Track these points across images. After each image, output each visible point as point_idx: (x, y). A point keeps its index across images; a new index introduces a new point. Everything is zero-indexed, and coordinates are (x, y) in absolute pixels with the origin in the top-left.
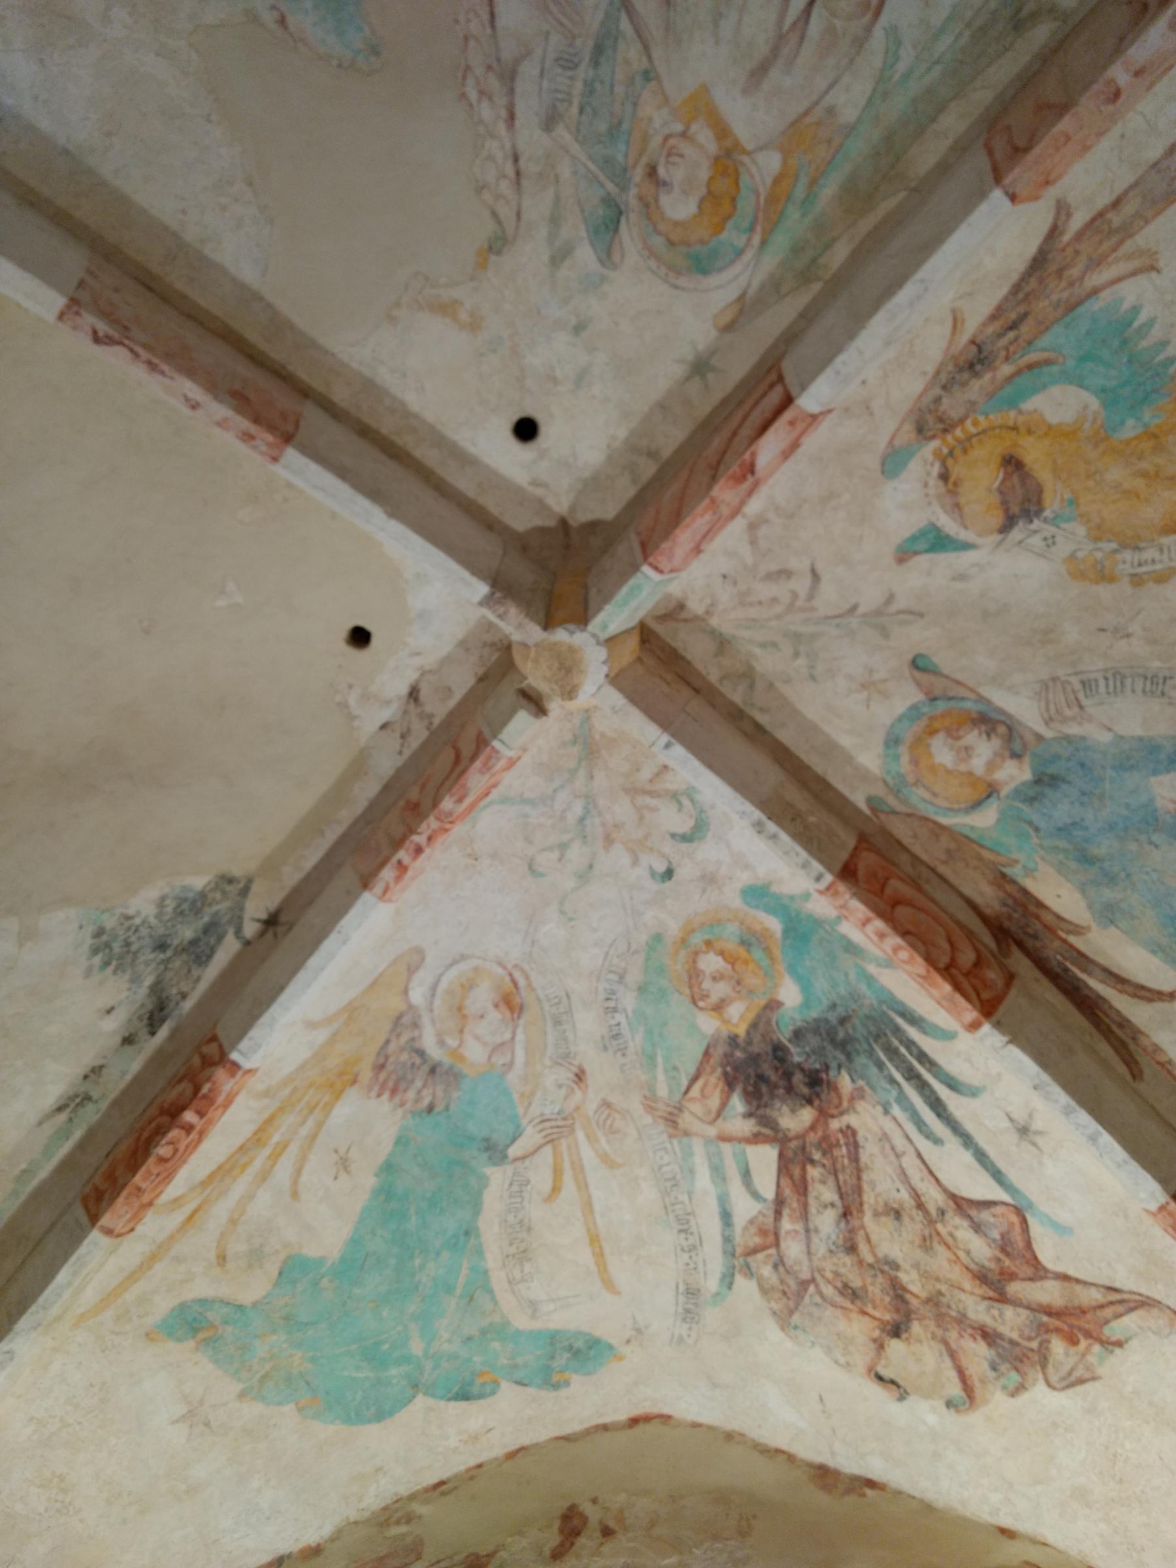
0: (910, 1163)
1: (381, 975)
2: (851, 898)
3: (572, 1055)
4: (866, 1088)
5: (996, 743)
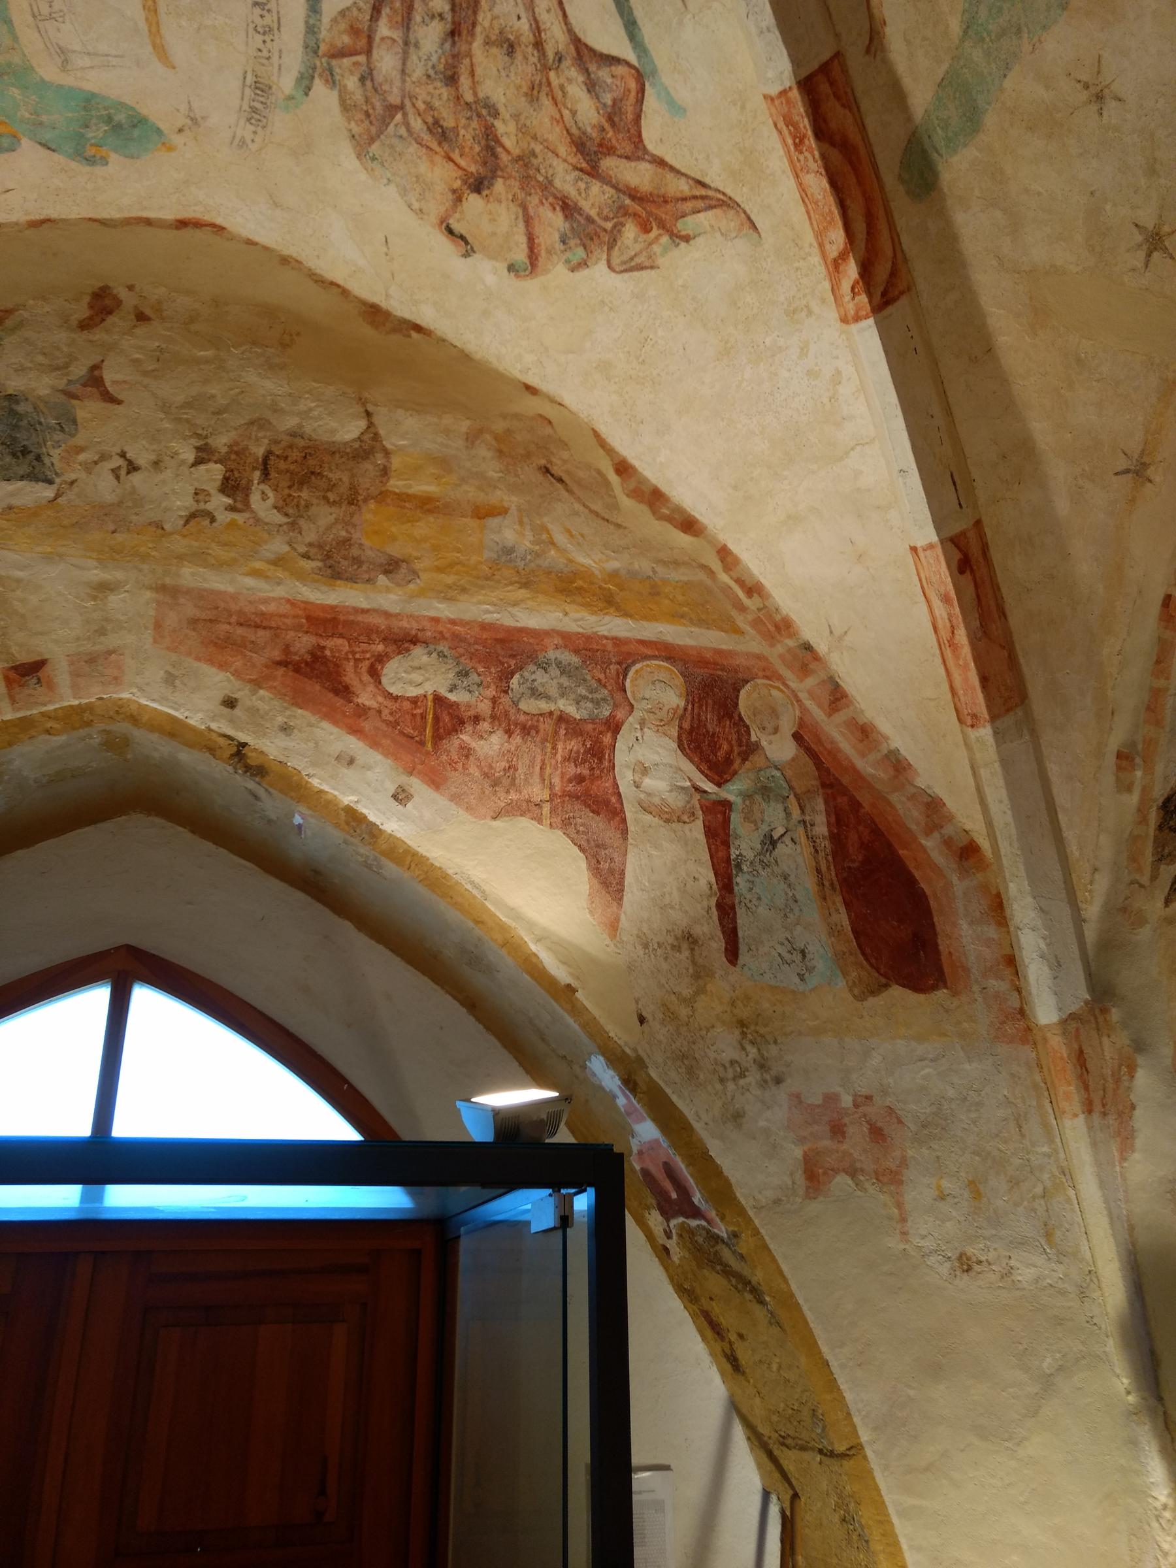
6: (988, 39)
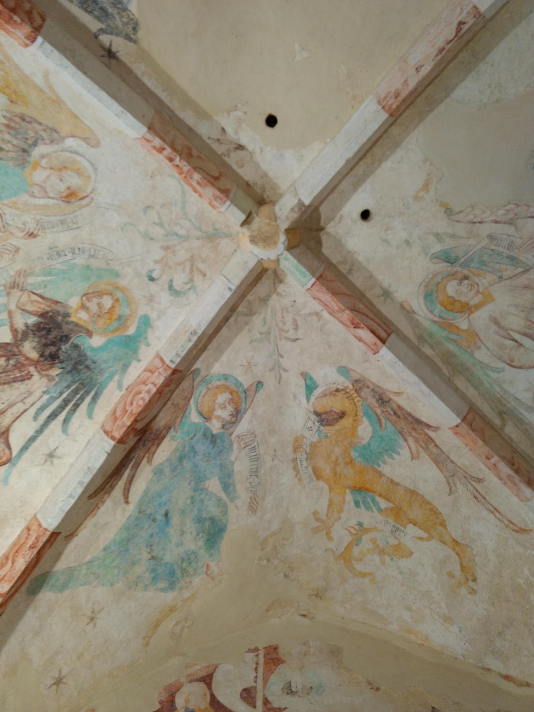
0: (19, 407)
1: (82, 121)
2: (164, 376)
3: (44, 231)
4: (55, 382)
5: (228, 418)
6: (90, 571)
